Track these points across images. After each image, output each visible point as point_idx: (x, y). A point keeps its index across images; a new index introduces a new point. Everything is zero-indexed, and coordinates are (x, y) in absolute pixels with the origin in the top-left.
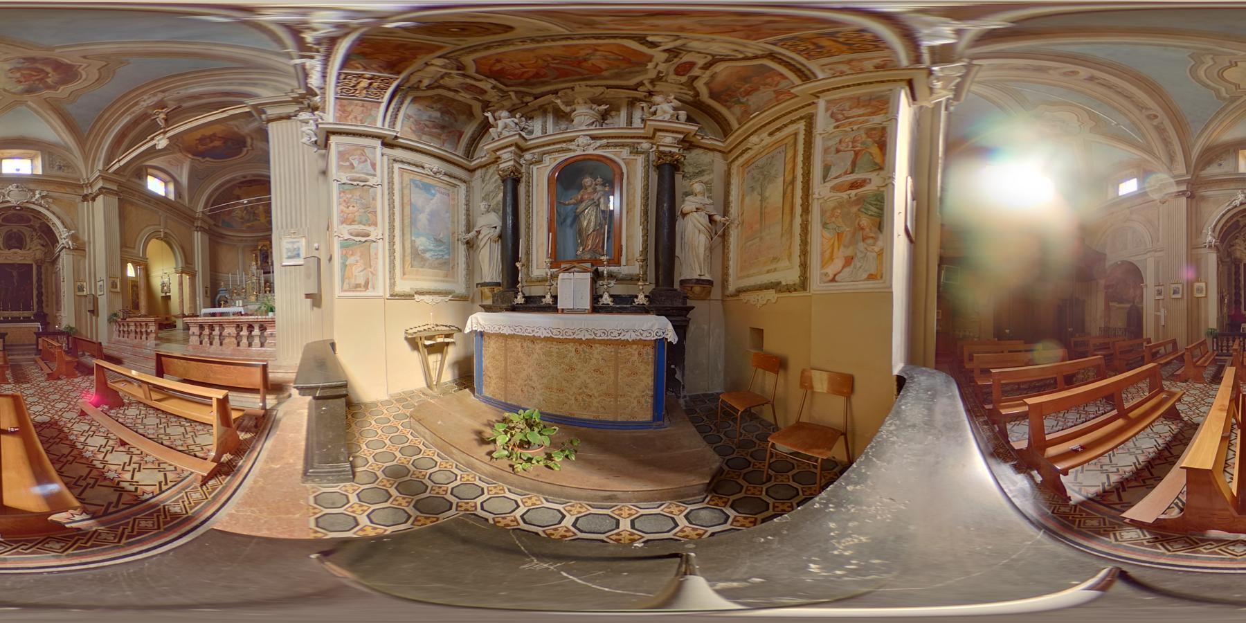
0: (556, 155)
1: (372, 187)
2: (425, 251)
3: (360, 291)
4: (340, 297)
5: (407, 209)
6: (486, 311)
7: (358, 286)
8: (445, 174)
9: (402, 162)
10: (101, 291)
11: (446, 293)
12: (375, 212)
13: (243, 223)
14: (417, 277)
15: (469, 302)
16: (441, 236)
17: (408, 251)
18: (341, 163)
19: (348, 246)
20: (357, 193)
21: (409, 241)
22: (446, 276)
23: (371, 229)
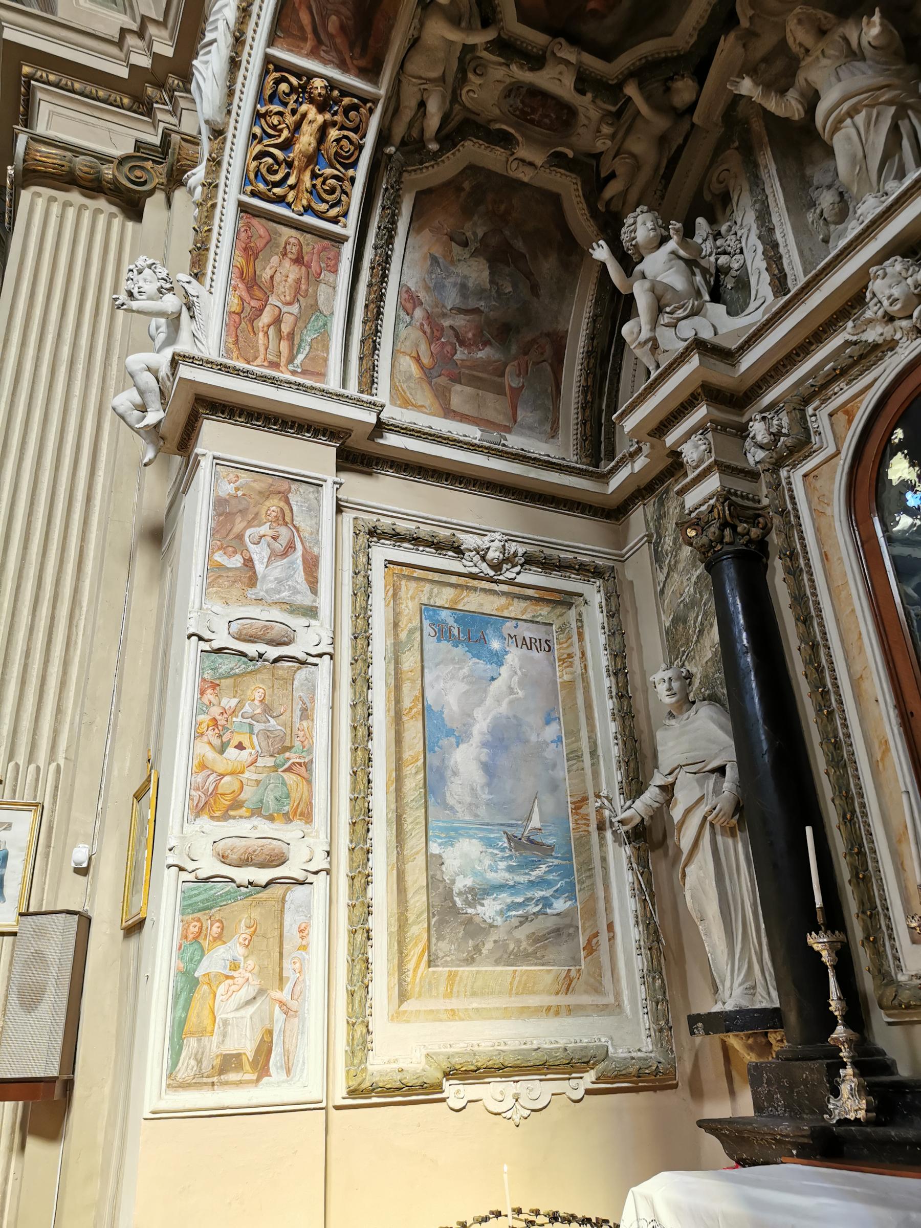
0: (844, 393)
1: (303, 663)
2: (477, 894)
3: (239, 1083)
4: (158, 1116)
5: (413, 731)
7: (230, 1063)
8: (529, 561)
9: (396, 537)
12: (308, 766)
14: (454, 1004)
15: (683, 1092)
16: (535, 822)
17: (418, 901)
18: (219, 557)
20: (256, 690)
21: (421, 860)
22: (568, 985)
23: (290, 832)
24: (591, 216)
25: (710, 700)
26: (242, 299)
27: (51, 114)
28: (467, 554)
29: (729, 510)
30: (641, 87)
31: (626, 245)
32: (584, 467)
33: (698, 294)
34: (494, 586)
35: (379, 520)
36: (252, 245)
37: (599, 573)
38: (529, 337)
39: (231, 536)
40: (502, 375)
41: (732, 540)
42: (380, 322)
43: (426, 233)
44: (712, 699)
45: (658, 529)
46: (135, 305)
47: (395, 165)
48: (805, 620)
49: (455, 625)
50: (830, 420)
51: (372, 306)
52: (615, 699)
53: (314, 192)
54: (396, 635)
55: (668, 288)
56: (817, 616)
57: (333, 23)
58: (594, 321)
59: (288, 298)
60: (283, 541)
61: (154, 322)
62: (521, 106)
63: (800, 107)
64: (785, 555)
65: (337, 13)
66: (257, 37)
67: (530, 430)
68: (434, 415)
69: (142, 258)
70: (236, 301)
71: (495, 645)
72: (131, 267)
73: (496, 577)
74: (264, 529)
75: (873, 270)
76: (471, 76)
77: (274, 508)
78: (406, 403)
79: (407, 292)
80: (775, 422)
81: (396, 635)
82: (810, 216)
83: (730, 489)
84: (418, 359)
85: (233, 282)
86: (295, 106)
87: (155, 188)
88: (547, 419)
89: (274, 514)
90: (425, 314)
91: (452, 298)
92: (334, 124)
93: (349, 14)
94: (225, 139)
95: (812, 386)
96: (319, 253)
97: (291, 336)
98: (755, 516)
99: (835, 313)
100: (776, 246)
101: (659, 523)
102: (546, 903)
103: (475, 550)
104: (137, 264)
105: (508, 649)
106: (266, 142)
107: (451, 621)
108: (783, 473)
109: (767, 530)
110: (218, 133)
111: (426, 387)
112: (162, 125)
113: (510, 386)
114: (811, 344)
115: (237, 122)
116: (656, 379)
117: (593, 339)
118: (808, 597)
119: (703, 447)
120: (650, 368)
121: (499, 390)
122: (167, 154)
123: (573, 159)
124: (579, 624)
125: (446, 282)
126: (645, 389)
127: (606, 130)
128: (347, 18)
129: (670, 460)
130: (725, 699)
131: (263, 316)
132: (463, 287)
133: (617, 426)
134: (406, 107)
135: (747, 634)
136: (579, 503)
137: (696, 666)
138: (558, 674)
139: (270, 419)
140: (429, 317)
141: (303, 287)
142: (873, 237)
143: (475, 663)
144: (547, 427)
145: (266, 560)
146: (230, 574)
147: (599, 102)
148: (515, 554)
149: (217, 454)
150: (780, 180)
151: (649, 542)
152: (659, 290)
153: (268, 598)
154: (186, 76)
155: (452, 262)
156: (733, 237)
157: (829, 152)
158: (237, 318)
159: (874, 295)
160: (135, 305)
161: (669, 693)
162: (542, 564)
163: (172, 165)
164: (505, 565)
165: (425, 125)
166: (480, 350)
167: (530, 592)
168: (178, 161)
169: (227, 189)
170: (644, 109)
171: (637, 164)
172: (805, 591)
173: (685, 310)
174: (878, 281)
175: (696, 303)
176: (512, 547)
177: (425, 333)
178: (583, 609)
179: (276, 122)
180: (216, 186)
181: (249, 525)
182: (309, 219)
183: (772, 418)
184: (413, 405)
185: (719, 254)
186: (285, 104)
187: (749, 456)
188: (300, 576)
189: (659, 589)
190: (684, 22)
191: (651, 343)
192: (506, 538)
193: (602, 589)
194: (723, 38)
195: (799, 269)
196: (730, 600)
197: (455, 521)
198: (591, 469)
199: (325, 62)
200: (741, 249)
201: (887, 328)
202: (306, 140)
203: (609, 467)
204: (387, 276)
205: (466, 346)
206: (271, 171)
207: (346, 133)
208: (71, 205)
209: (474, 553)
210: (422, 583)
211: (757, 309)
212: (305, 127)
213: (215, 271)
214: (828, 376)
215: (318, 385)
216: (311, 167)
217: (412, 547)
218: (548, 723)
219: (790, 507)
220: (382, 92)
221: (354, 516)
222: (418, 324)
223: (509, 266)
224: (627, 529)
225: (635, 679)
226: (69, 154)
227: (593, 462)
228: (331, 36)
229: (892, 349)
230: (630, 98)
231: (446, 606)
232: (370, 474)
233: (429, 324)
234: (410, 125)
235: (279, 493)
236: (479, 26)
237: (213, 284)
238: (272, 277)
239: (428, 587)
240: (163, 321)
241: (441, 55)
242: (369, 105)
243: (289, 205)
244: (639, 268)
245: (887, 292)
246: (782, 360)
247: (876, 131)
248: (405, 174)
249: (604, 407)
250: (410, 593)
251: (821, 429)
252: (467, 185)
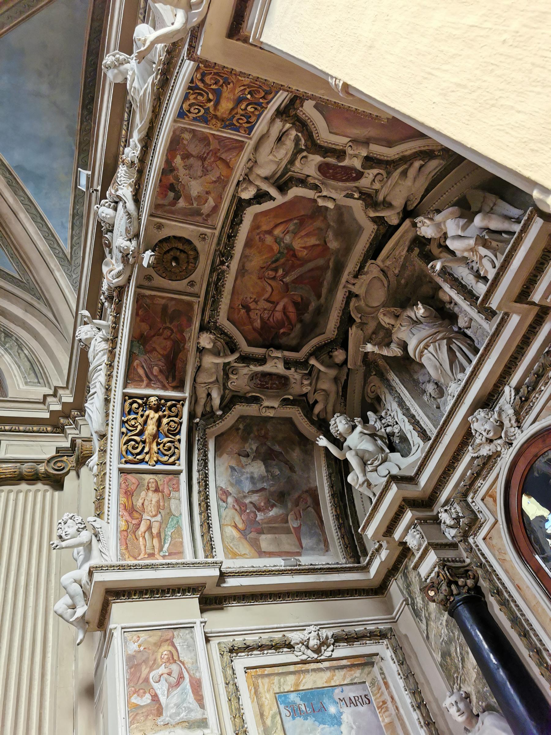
0: (484, 486)
8: (337, 639)
9: (248, 649)
18: (135, 700)
24: (311, 424)
25: (488, 710)
26: (127, 521)
28: (296, 647)
29: (449, 572)
30: (317, 359)
31: (335, 435)
32: (352, 565)
33: (382, 450)
34: (320, 665)
35: (234, 640)
36: (129, 489)
37: (384, 635)
38: (296, 495)
39: (141, 681)
40: (287, 522)
41: (458, 591)
42: (209, 511)
43: (225, 456)
44: (489, 708)
46: (64, 544)
47: (200, 427)
48: (525, 635)
49: (302, 703)
50: (483, 503)
51: (203, 503)
52: (424, 728)
53: (160, 452)
54: (264, 723)
55: (365, 451)
56: (531, 629)
57: (156, 370)
58: (330, 477)
59: (154, 513)
60: (175, 674)
61: (76, 550)
62: (259, 382)
63: (399, 350)
64: (494, 593)
65: (157, 365)
66: (117, 386)
68: (253, 558)
69: (66, 514)
70: (124, 523)
71: (332, 710)
72: (60, 521)
73: (319, 658)
74: (162, 670)
75: (470, 419)
76: (231, 376)
77: (165, 653)
78: (235, 555)
79: (221, 490)
80: (453, 511)
81: (264, 723)
82: (425, 398)
83: (444, 558)
84: (236, 527)
85: (120, 513)
86: (142, 413)
87: (69, 470)
88: (320, 541)
89: (166, 657)
90: (234, 499)
91: (247, 486)
92: (164, 416)
93: (163, 364)
94: (107, 439)
95: (465, 486)
96: (168, 483)
97: (159, 534)
98: (465, 572)
99: (459, 444)
100: (413, 417)
101: (409, 590)
103: (301, 642)
104: (64, 519)
105: (341, 711)
106: (129, 434)
107: (298, 701)
108: (471, 540)
109: (476, 578)
110: (103, 436)
111: (244, 541)
112: (70, 437)
113: (293, 527)
114: (454, 463)
115: (112, 428)
116: (376, 503)
117: (332, 487)
118: (519, 618)
119: (418, 536)
120: (371, 497)
121: (288, 531)
122: (75, 450)
123: (293, 400)
124: (383, 676)
125: (242, 478)
126: (372, 510)
127: (306, 382)
128: (162, 366)
129: (401, 548)
130: (496, 705)
131: (140, 528)
132: (252, 478)
133: (363, 535)
134: (201, 398)
135: (493, 654)
136: (356, 590)
137: (469, 686)
138: (380, 719)
139: (154, 592)
140: (237, 500)
141: (162, 504)
142: (463, 402)
143: (323, 729)
144: (322, 546)
145: (166, 692)
146: (144, 710)
147: (298, 371)
148: (327, 638)
149: (124, 625)
150: (403, 384)
151: (408, 604)
152: (360, 454)
153: (172, 721)
154: (82, 411)
155: (243, 467)
156: (390, 417)
157: (422, 366)
158: (125, 533)
159: (476, 431)
160: (64, 544)
161: (458, 713)
162: (346, 639)
163: (78, 456)
164: (322, 648)
165: (213, 404)
166: (270, 511)
167: (344, 662)
168: (82, 452)
169: (111, 464)
170: (322, 368)
171: (327, 394)
172: (516, 614)
173: (378, 461)
174: (475, 424)
175: (383, 455)
176: (324, 633)
177: (236, 510)
178: (382, 664)
179: (133, 423)
180: (105, 463)
181: (151, 669)
182: (159, 467)
183: (450, 509)
184: (239, 555)
185: (386, 427)
186: (137, 413)
187: (446, 534)
188: (191, 698)
189: (425, 636)
190: (328, 327)
191: (366, 483)
192: (318, 628)
193: (389, 646)
194: (350, 328)
195: (431, 426)
196: (473, 634)
197: (282, 625)
198: (356, 565)
199: (154, 388)
200: (396, 422)
201: (491, 446)
202: (151, 428)
203: (366, 561)
204: (208, 485)
205: (262, 511)
206: (134, 448)
207: (171, 419)
208: (21, 492)
209: (301, 645)
210: (272, 677)
211: (417, 450)
212: (149, 421)
213: (110, 509)
214: (471, 478)
215: (180, 561)
216: (156, 440)
217: (259, 652)
219: (483, 561)
220: (187, 395)
221: (218, 641)
222: (231, 506)
223: (274, 460)
224: (390, 598)
225: (433, 707)
226: (19, 464)
227: (356, 560)
228: (156, 376)
229: (499, 456)
230: (313, 365)
231: (292, 689)
232: (222, 609)
233: (238, 504)
234: (205, 406)
235: (167, 640)
236: (230, 353)
237: (109, 517)
238: (143, 504)
239: (276, 678)
240: (81, 548)
241: (214, 370)
242: (181, 402)
243: (147, 462)
244: (345, 444)
245: (483, 428)
246: (442, 475)
247: (441, 353)
248: (207, 430)
249: (351, 524)
250: (266, 687)
251: (480, 509)
252: (241, 426)
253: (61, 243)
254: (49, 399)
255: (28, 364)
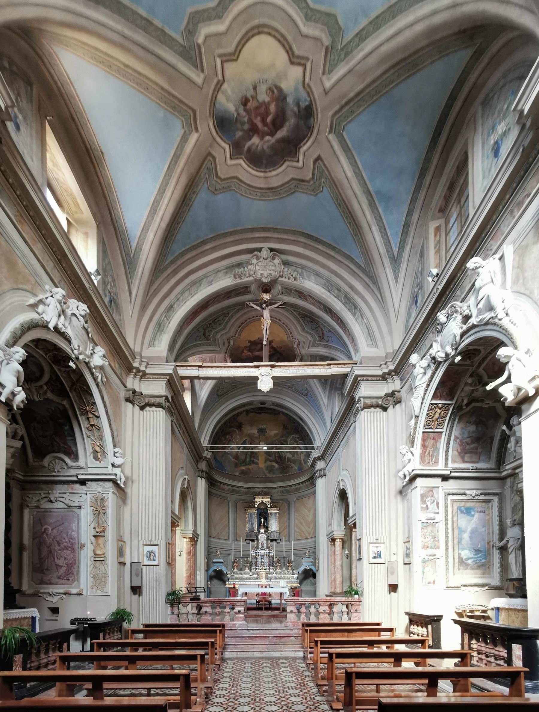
2: (468, 559)
6: (510, 598)
8: (481, 494)
9: (453, 494)
10: (149, 559)
11: (483, 585)
13: (236, 465)
16: (479, 546)
17: (457, 560)
19: (425, 562)
20: (430, 528)
22: (484, 574)
27: (365, 387)
43: (461, 423)
45: (513, 484)
57: (444, 393)
67: (484, 461)
71: (473, 513)
74: (429, 499)
84: (457, 451)
97: (432, 455)
102: (480, 560)
121: (476, 453)
140: (460, 441)
218: (483, 527)
253: (393, 246)
254: (383, 366)
255: (367, 330)
